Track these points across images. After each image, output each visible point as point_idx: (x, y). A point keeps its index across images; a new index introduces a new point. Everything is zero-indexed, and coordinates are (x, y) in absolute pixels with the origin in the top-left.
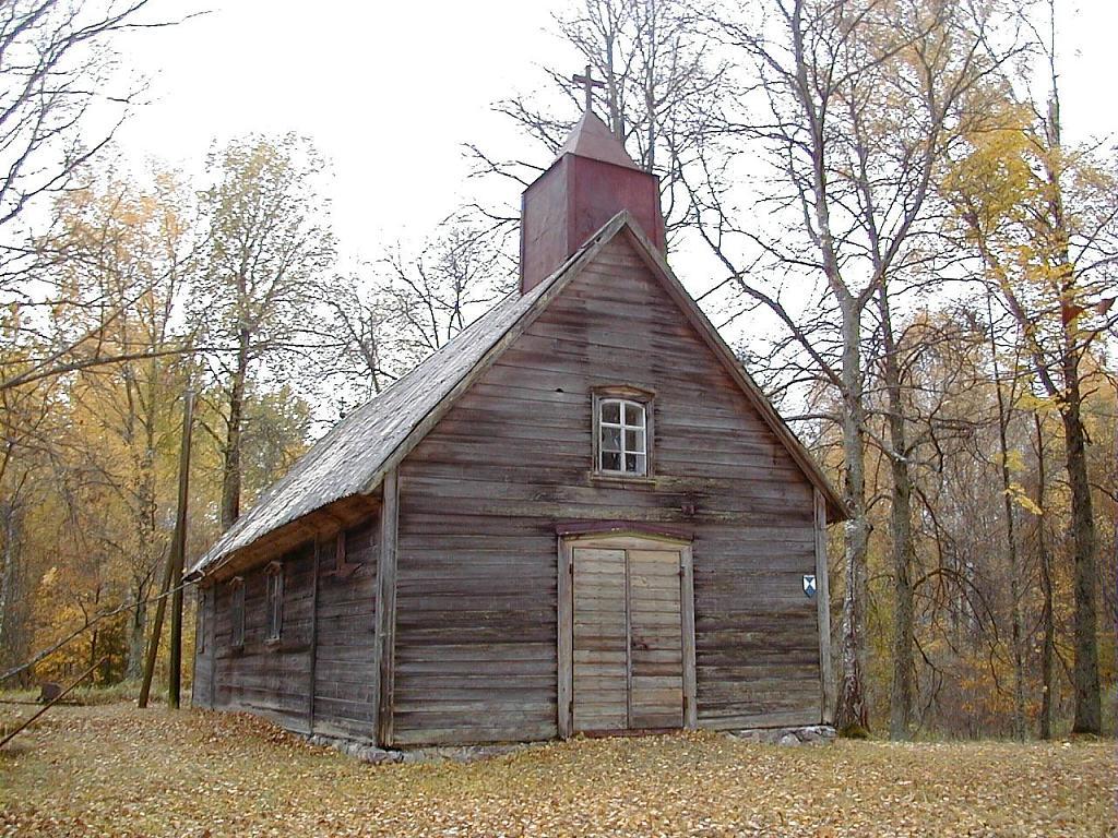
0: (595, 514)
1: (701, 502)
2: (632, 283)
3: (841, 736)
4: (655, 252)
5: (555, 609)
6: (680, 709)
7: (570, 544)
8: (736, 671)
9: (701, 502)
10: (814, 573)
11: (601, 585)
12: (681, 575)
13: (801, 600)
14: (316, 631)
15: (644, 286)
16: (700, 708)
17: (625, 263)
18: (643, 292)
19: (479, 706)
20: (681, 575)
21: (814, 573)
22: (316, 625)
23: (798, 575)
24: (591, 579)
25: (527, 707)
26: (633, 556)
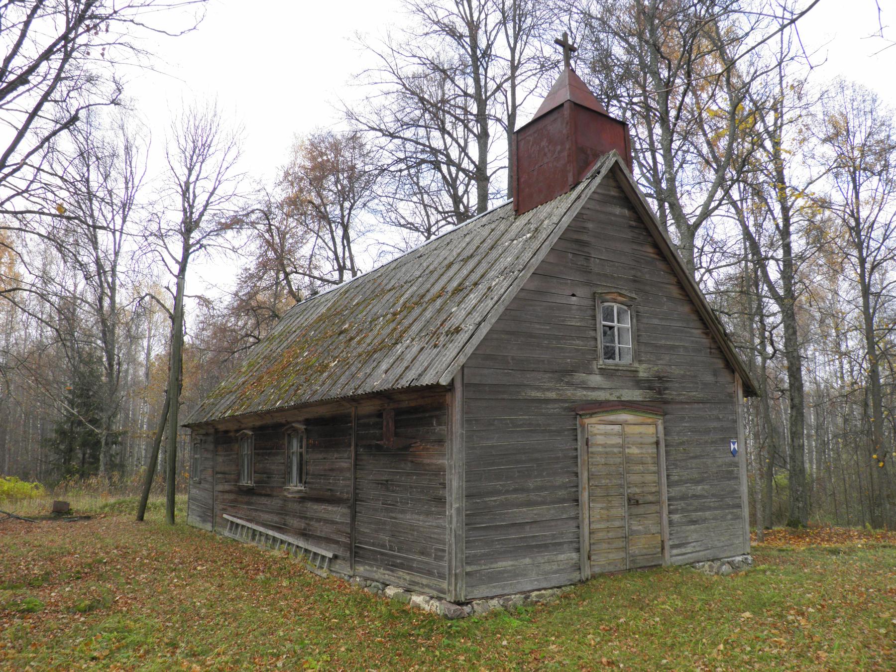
0: (602, 396)
1: (667, 385)
2: (618, 210)
3: (55, 505)
4: (626, 171)
5: (576, 474)
6: (659, 550)
7: (587, 421)
8: (694, 516)
9: (667, 385)
10: (736, 438)
11: (607, 453)
12: (657, 443)
13: (729, 459)
14: (355, 488)
15: (626, 212)
16: (658, 502)
17: (613, 193)
18: (623, 217)
19: (527, 561)
20: (657, 443)
21: (736, 438)
22: (355, 484)
23: (726, 441)
24: (600, 449)
25: (562, 557)
26: (629, 429)
